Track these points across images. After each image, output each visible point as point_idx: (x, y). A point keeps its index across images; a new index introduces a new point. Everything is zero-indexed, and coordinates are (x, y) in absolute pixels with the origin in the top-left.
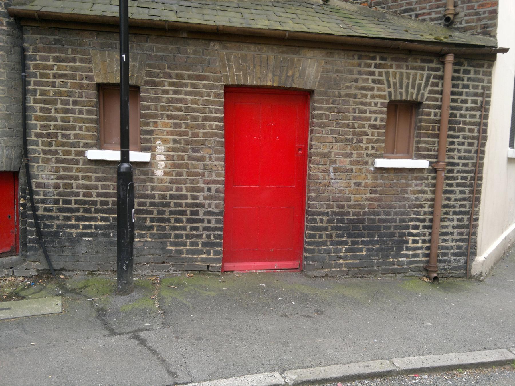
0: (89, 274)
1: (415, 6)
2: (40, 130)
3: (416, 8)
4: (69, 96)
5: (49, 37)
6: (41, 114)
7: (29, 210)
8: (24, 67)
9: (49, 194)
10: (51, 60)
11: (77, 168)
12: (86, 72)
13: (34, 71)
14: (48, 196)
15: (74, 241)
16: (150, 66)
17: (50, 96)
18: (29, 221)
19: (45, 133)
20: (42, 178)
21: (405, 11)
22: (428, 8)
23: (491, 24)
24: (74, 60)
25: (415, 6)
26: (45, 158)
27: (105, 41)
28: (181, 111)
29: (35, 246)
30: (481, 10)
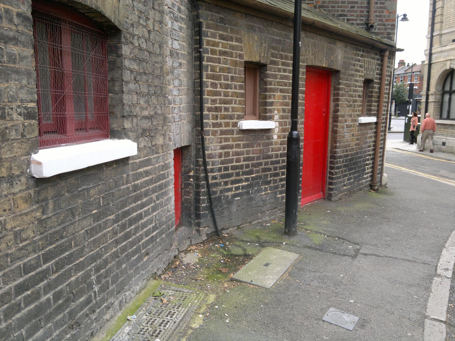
0: (237, 229)
1: (347, 13)
2: (211, 104)
3: (347, 15)
4: (229, 73)
5: (216, 15)
6: (212, 89)
7: (202, 181)
8: (200, 42)
9: (216, 164)
10: (218, 38)
11: (233, 138)
12: (239, 51)
13: (207, 47)
14: (215, 166)
15: (230, 202)
16: (274, 48)
17: (216, 72)
18: (203, 190)
19: (213, 107)
20: (211, 149)
21: (340, 15)
22: (355, 16)
23: (392, 32)
24: (231, 39)
25: (347, 13)
26: (214, 130)
27: (250, 23)
28: (286, 86)
29: (206, 213)
30: (387, 23)
